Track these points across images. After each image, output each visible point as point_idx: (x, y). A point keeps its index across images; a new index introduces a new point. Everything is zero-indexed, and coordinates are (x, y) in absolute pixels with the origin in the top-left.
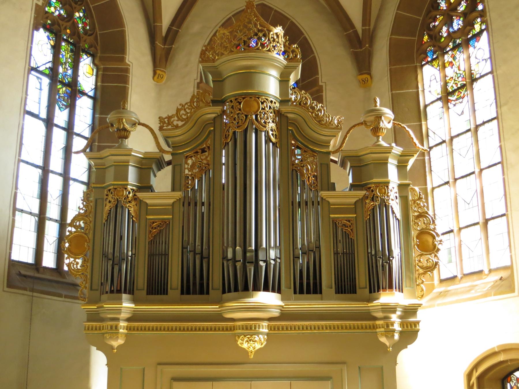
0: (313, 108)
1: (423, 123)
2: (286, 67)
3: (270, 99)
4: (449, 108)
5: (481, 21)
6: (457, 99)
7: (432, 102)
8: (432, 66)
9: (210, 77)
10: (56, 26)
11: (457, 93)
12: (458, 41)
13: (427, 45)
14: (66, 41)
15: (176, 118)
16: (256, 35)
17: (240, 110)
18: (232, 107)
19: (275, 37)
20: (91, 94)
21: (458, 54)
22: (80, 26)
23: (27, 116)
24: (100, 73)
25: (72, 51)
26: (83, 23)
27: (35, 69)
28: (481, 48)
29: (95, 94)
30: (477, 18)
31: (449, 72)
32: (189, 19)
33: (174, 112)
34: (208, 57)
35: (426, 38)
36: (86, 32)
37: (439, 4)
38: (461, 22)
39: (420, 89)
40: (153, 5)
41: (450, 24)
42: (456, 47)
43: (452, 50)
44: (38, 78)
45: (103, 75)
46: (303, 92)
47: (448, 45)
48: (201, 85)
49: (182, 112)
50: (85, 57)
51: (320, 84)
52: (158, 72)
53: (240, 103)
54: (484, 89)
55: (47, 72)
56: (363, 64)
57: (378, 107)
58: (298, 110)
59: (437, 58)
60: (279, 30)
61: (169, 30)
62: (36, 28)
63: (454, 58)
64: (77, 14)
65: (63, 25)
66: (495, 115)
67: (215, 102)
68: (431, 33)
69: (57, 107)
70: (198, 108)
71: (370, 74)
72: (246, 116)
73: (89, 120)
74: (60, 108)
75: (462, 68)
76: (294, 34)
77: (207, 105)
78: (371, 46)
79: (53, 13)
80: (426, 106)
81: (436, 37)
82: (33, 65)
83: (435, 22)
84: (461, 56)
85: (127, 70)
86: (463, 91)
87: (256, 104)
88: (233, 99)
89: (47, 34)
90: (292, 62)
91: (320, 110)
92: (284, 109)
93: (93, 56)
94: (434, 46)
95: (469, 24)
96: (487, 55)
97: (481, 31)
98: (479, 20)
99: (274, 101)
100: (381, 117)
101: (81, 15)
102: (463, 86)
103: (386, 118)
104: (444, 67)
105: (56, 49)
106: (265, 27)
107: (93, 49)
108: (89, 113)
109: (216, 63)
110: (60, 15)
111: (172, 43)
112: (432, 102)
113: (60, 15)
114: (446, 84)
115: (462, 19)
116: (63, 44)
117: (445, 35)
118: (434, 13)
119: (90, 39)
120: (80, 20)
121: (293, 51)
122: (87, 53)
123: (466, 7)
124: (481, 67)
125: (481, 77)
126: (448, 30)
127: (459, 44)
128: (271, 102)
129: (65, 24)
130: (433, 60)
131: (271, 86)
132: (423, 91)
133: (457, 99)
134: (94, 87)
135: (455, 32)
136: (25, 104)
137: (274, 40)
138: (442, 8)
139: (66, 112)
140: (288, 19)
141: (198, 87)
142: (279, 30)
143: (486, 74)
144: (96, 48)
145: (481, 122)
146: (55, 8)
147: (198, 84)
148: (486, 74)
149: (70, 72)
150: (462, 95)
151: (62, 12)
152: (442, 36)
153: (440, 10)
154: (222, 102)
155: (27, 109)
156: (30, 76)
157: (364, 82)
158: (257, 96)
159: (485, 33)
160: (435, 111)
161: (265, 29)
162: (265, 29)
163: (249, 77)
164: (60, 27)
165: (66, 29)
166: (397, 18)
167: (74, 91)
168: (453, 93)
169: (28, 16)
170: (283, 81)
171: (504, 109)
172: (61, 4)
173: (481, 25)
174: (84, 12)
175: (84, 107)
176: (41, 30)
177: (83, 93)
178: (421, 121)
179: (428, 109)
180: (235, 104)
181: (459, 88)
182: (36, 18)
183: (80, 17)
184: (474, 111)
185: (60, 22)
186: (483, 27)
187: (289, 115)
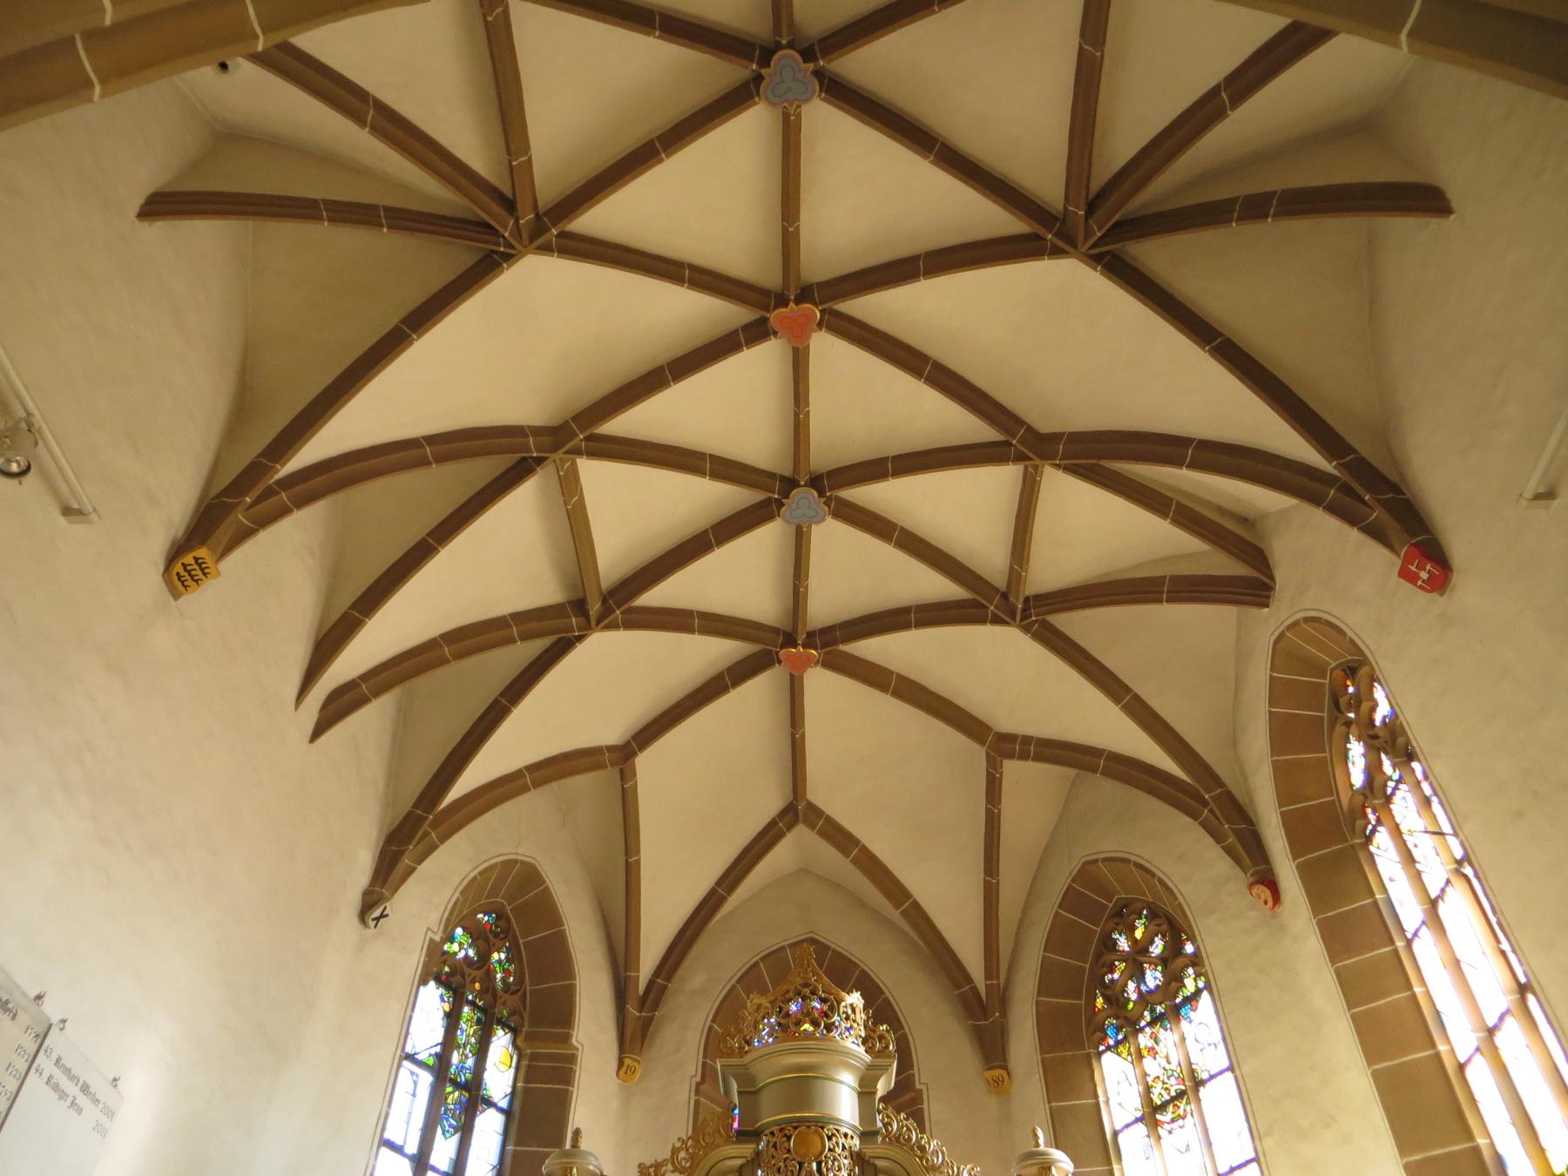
0: (923, 1149)
1: (1115, 1167)
2: (870, 1067)
3: (844, 1130)
4: (1159, 1138)
6: (1173, 1121)
7: (1127, 1126)
8: (1119, 1054)
9: (734, 1086)
10: (458, 978)
11: (1171, 1108)
12: (1159, 1009)
13: (1104, 1014)
14: (473, 1004)
15: (670, 1167)
16: (799, 993)
17: (789, 1151)
18: (775, 1146)
20: (504, 1104)
21: (1162, 1034)
22: (499, 976)
23: (384, 1150)
24: (525, 1063)
25: (479, 1022)
26: (506, 971)
27: (411, 1058)
28: (1202, 1023)
29: (511, 1103)
31: (1152, 1066)
32: (686, 964)
33: (668, 1155)
34: (732, 1048)
35: (1100, 1001)
36: (506, 987)
37: (1115, 942)
38: (1159, 975)
39: (1101, 1099)
41: (1140, 977)
42: (1156, 1020)
43: (1149, 1024)
44: (412, 1073)
45: (529, 1067)
46: (903, 1115)
47: (1142, 1017)
48: (703, 1087)
49: (682, 1154)
50: (500, 1032)
51: (918, 1086)
52: (627, 1061)
53: (789, 1138)
54: (1221, 1098)
55: (431, 1062)
56: (992, 1048)
57: (1042, 1148)
58: (894, 1152)
59: (1125, 1038)
60: (855, 999)
61: (651, 983)
62: (424, 981)
63: (1156, 1041)
64: (495, 956)
66: (1252, 1155)
67: (744, 1136)
68: (1108, 993)
69: (439, 1131)
70: (712, 1147)
71: (1005, 1068)
72: (801, 1164)
73: (493, 1158)
74: (444, 1133)
75: (1174, 1061)
76: (881, 1010)
77: (728, 1141)
78: (1004, 1014)
79: (455, 954)
80: (1116, 1134)
81: (1118, 1001)
82: (409, 1050)
83: (1112, 972)
84: (1167, 1037)
85: (572, 1059)
86: (1182, 1105)
87: (818, 1140)
88: (775, 1129)
89: (441, 990)
91: (935, 1153)
92: (870, 1151)
93: (514, 1031)
94: (1117, 1018)
95: (1174, 980)
96: (1217, 1036)
97: (1198, 992)
98: (1190, 971)
99: (850, 1133)
100: (1049, 1169)
101: (503, 956)
102: (1181, 1095)
103: (1059, 1169)
104: (1140, 1057)
105: (452, 1018)
107: (515, 1018)
108: (496, 1140)
109: (747, 1059)
110: (466, 956)
111: (655, 1007)
112: (1127, 1126)
113: (466, 956)
114: (1148, 1089)
116: (466, 1009)
117: (1134, 997)
118: (1108, 957)
119: (513, 1000)
121: (881, 1038)
122: (504, 1025)
124: (1210, 1056)
125: (1212, 1077)
126: (1138, 987)
127: (1162, 1015)
128: (846, 1135)
129: (474, 973)
130: (1118, 1043)
131: (844, 1104)
132: (1107, 1102)
133: (1173, 1121)
134: (509, 1090)
135: (1150, 992)
136: (383, 1129)
137: (847, 1018)
139: (455, 1140)
140: (856, 966)
141: (697, 1092)
142: (855, 999)
143: (1221, 1073)
144: (522, 1017)
145: (1227, 1169)
146: (461, 944)
147: (698, 1085)
148: (1221, 1073)
149: (470, 1062)
150: (1181, 1112)
151: (471, 953)
152: (1128, 1000)
154: (756, 1135)
155: (387, 1135)
156: (402, 1070)
157: (997, 1084)
158: (821, 1123)
159: (1205, 996)
160: (1133, 1142)
163: (804, 1087)
165: (473, 981)
166: (1046, 968)
167: (475, 1098)
168: (1163, 1107)
169: (414, 960)
170: (865, 1092)
171: (1268, 1143)
174: (508, 951)
175: (489, 1128)
176: (432, 984)
177: (490, 1103)
178: (1110, 1164)
179: (1121, 1138)
180: (778, 1138)
181: (1173, 1099)
182: (426, 965)
183: (500, 961)
184: (1210, 1144)
185: (467, 970)
186: (1201, 985)
187: (879, 1163)
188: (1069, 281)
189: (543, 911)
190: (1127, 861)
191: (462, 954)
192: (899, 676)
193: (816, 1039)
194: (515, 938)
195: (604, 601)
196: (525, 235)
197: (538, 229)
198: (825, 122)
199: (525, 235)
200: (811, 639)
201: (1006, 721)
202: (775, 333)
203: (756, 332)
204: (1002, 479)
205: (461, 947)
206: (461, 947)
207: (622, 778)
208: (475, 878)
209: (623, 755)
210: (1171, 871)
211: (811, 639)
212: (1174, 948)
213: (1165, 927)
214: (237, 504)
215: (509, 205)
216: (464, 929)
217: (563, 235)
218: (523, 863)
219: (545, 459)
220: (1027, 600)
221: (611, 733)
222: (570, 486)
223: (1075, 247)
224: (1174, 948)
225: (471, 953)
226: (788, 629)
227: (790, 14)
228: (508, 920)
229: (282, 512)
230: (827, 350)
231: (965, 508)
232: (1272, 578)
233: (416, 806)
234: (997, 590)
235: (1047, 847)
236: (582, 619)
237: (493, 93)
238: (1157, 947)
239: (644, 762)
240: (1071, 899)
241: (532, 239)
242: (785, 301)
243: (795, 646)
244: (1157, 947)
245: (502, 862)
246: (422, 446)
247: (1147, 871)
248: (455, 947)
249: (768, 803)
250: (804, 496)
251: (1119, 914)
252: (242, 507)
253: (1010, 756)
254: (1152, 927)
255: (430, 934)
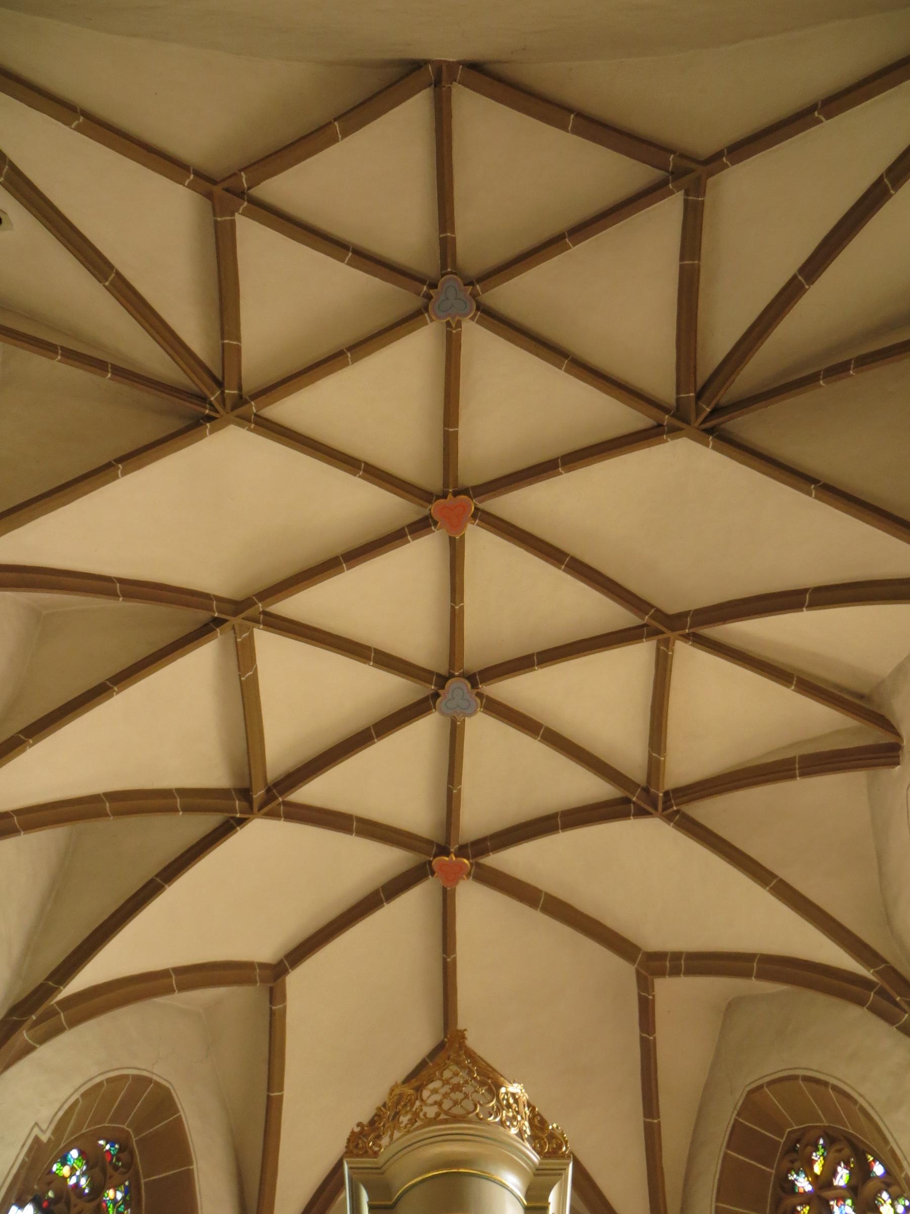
2: (539, 1172)
5: (890, 1197)
19: (511, 1101)
30: (880, 1191)
37: (793, 1183)
40: (260, 1190)
64: (111, 1194)
65: (75, 1206)
79: (64, 1179)
90: (550, 1157)
98: (885, 1195)
101: (119, 1196)
106: (489, 1078)
113: (77, 1185)
115: (849, 1202)
120: (114, 1206)
123: (851, 1174)
138: (801, 1190)
146: (73, 1170)
151: (83, 1182)
153: (799, 1193)
161: (490, 1081)
162: (490, 1081)
164: (69, 1209)
172: (87, 1164)
173: (893, 1205)
174: (126, 1192)
183: (115, 1201)
188: (683, 460)
189: (173, 1146)
190: (794, 1078)
191: (73, 1181)
192: (546, 894)
193: (470, 1122)
194: (137, 1173)
195: (269, 790)
196: (229, 404)
197: (270, 797)
198: (478, 339)
199: (229, 404)
200: (462, 851)
201: (654, 939)
202: (433, 873)
203: (421, 527)
204: (634, 661)
205: (72, 1171)
206: (72, 1171)
207: (272, 1002)
208: (100, 1084)
209: (272, 976)
210: (842, 1073)
211: (462, 851)
212: (862, 1173)
213: (847, 1151)
214: (23, 1022)
215: (220, 384)
216: (81, 1153)
217: (286, 804)
218: (157, 1084)
219: (225, 621)
220: (666, 794)
221: (265, 951)
222: (244, 658)
223: (688, 422)
224: (862, 1173)
225: (83, 1182)
226: (442, 842)
227: (454, 255)
228: (132, 1153)
229: (58, 1030)
230: (480, 543)
231: (601, 697)
232: (898, 735)
233: (49, 978)
234: (638, 786)
235: (707, 1087)
236: (245, 804)
237: (216, 295)
238: (842, 1177)
239: (294, 980)
240: (739, 1137)
241: (234, 408)
242: (446, 500)
243: (447, 854)
244: (842, 1177)
245: (134, 1076)
246: (170, 976)
247: (817, 1081)
248: (66, 1171)
249: (419, 1041)
250: (457, 688)
251: (793, 1149)
252: (28, 1023)
253: (662, 973)
254: (833, 1155)
255: (36, 1131)
